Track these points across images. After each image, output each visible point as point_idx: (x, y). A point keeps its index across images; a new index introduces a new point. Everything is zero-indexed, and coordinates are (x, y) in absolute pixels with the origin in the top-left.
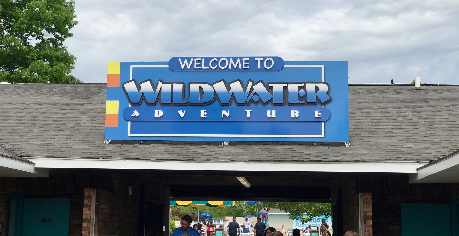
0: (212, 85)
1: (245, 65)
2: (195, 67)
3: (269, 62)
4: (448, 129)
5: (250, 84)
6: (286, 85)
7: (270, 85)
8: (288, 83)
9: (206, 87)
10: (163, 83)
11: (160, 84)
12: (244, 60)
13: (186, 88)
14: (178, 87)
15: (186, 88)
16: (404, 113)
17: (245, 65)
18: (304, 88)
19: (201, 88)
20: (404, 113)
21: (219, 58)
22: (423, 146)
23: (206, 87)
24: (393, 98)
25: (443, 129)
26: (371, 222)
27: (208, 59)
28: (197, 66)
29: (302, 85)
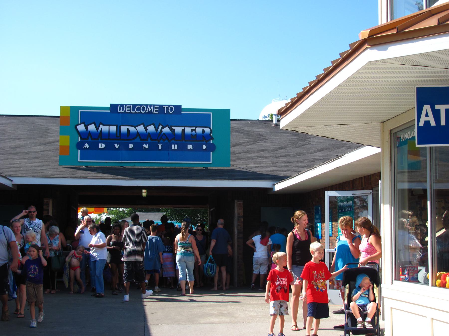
0: (135, 127)
1: (156, 111)
2: (127, 111)
3: (171, 109)
4: (294, 157)
5: (160, 127)
6: (183, 128)
7: (173, 128)
8: (185, 127)
9: (132, 129)
10: (103, 125)
11: (101, 126)
12: (155, 107)
13: (118, 129)
14: (113, 129)
15: (118, 129)
16: (265, 144)
17: (156, 111)
18: (195, 130)
19: (128, 129)
20: (265, 144)
21: (141, 105)
22: (277, 169)
23: (132, 129)
24: (257, 131)
25: (291, 157)
26: (242, 220)
27: (134, 106)
28: (128, 110)
29: (194, 128)
